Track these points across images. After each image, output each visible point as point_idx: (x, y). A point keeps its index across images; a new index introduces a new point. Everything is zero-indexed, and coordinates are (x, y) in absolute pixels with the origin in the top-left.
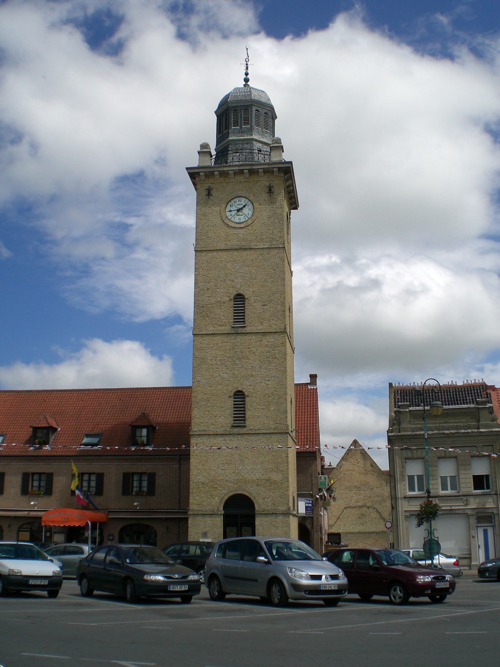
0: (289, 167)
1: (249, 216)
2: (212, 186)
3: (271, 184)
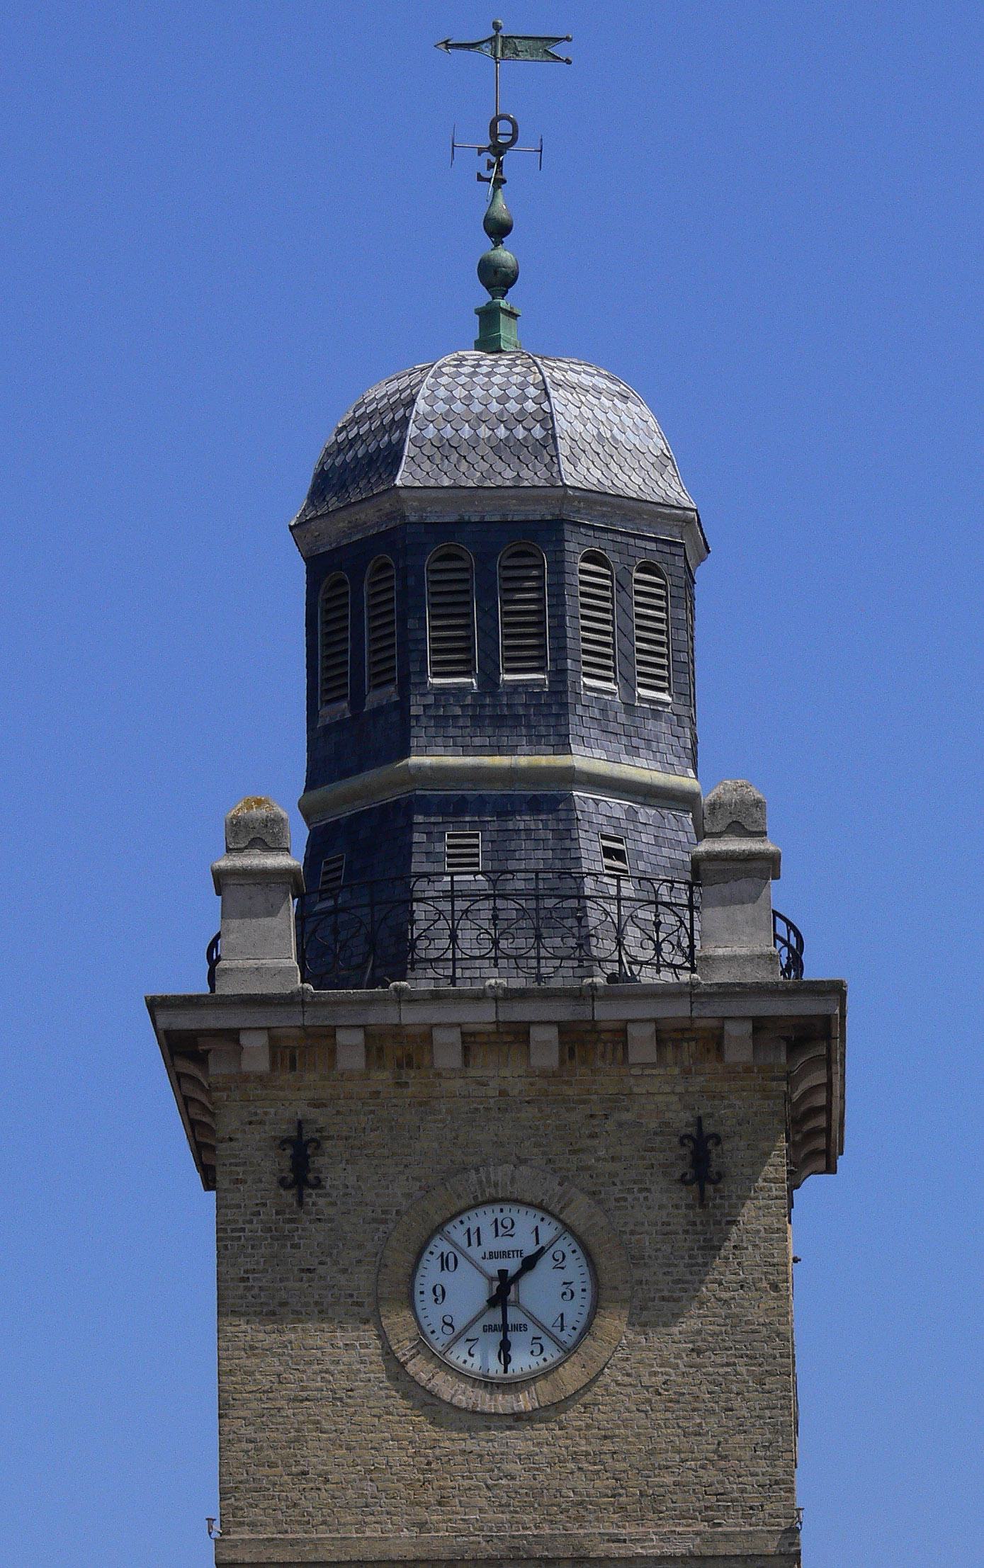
0: (827, 1019)
1: (563, 1336)
2: (320, 1117)
3: (705, 1123)
